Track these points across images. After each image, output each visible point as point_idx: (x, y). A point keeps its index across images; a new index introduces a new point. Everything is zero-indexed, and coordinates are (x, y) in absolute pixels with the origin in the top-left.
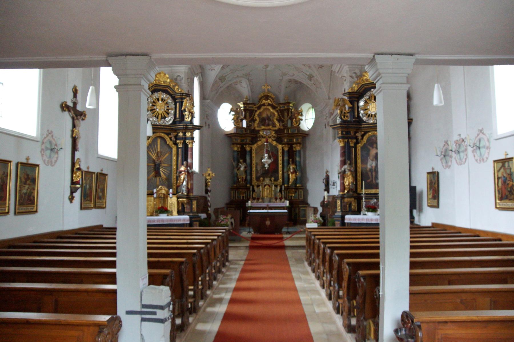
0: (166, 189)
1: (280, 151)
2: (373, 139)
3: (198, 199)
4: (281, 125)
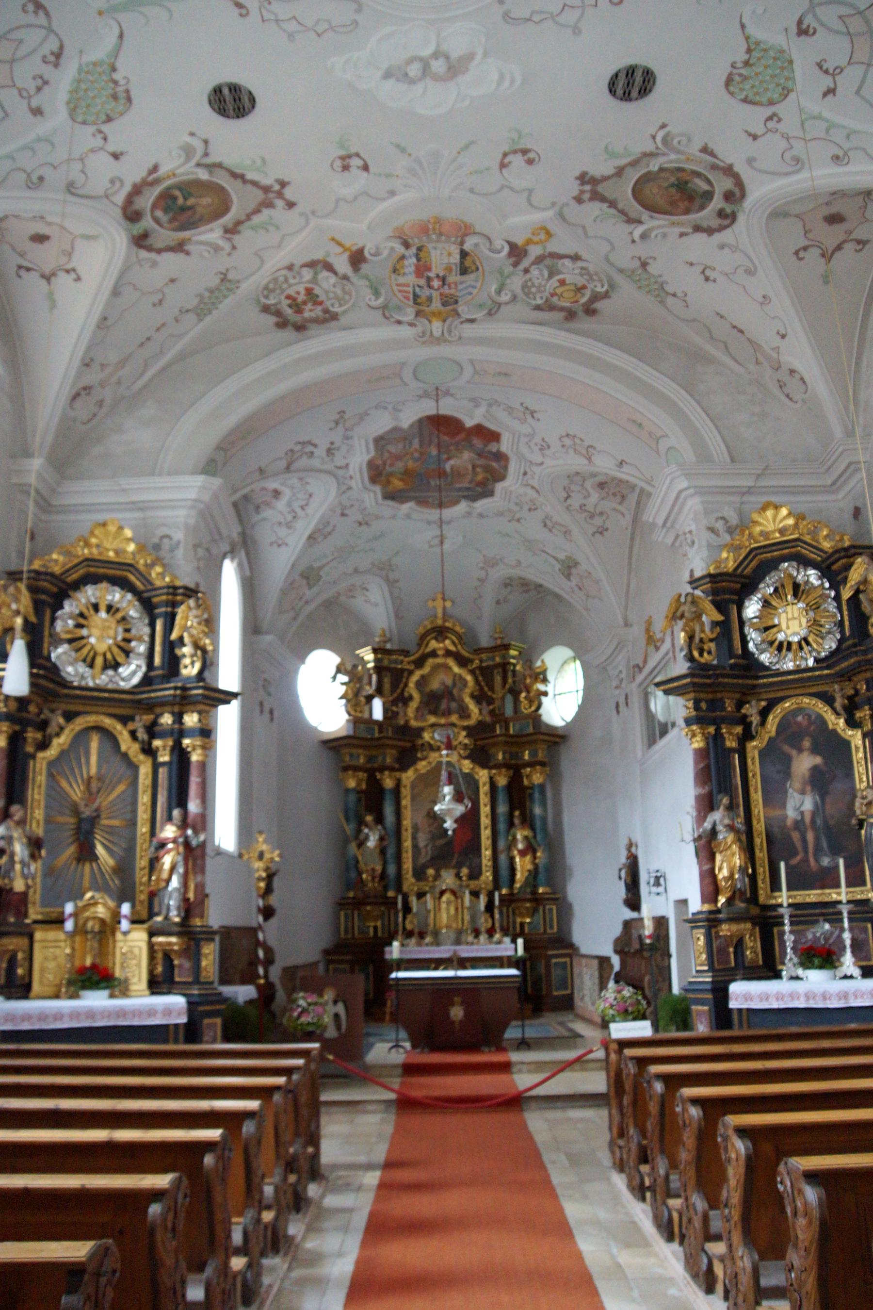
0: (111, 904)
1: (484, 790)
2: (799, 724)
3: (229, 936)
4: (485, 712)
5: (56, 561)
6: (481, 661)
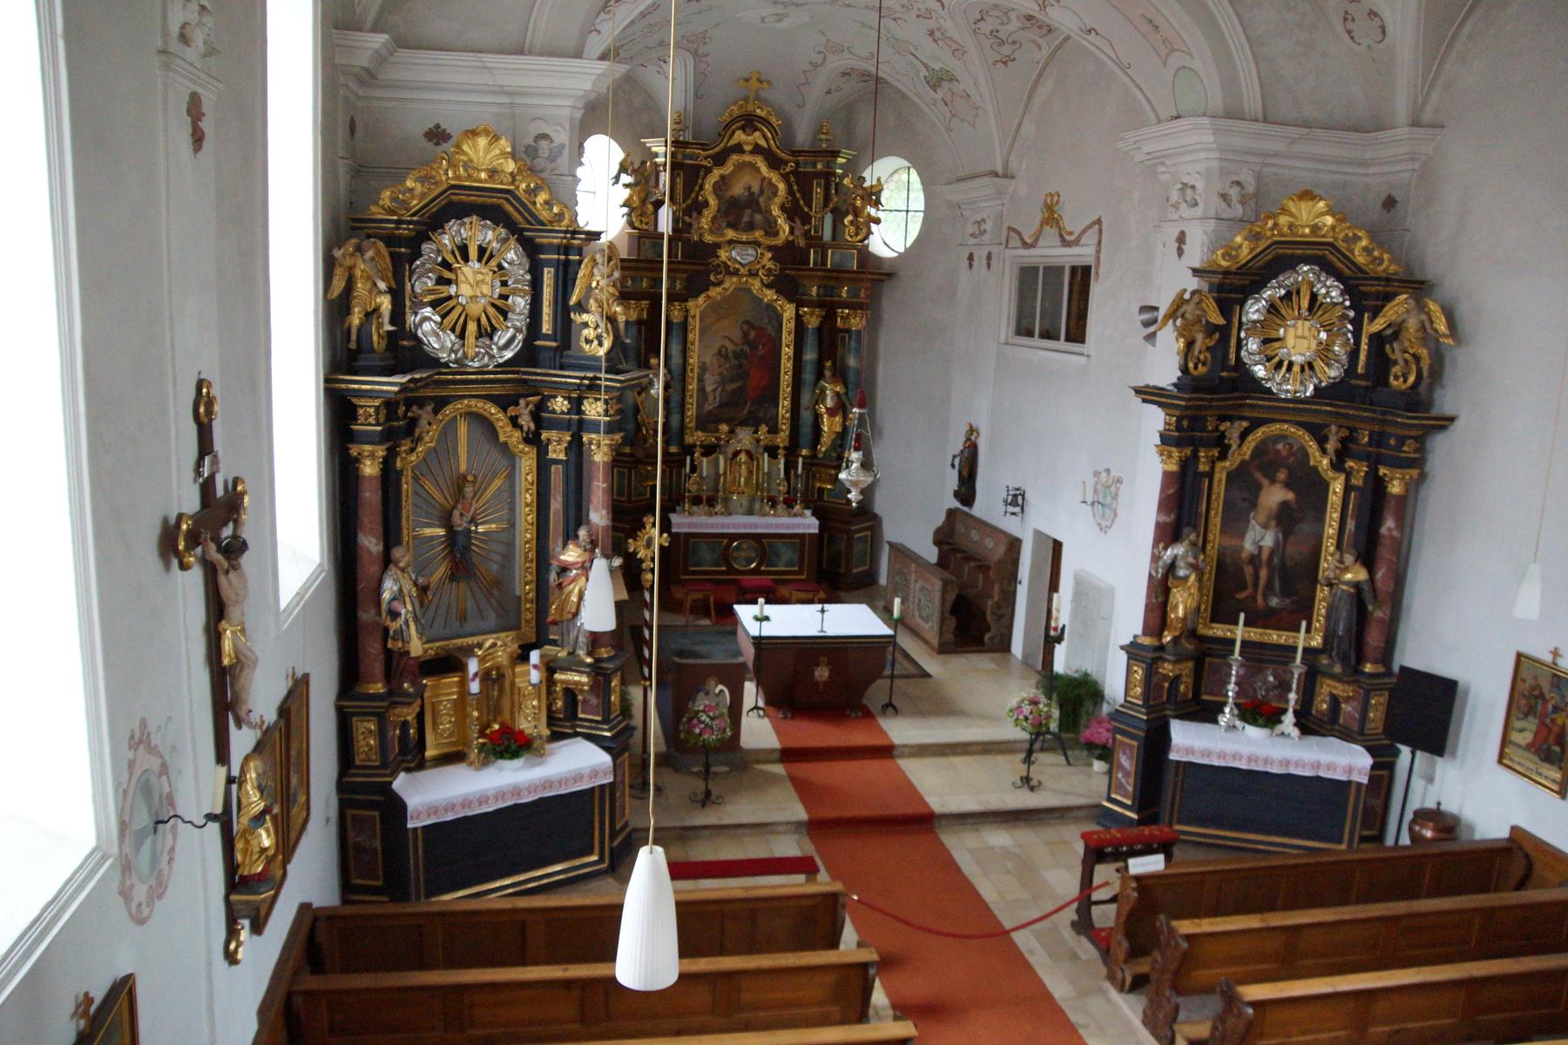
1: (788, 326)
2: (1278, 452)
5: (411, 190)
6: (797, 164)
